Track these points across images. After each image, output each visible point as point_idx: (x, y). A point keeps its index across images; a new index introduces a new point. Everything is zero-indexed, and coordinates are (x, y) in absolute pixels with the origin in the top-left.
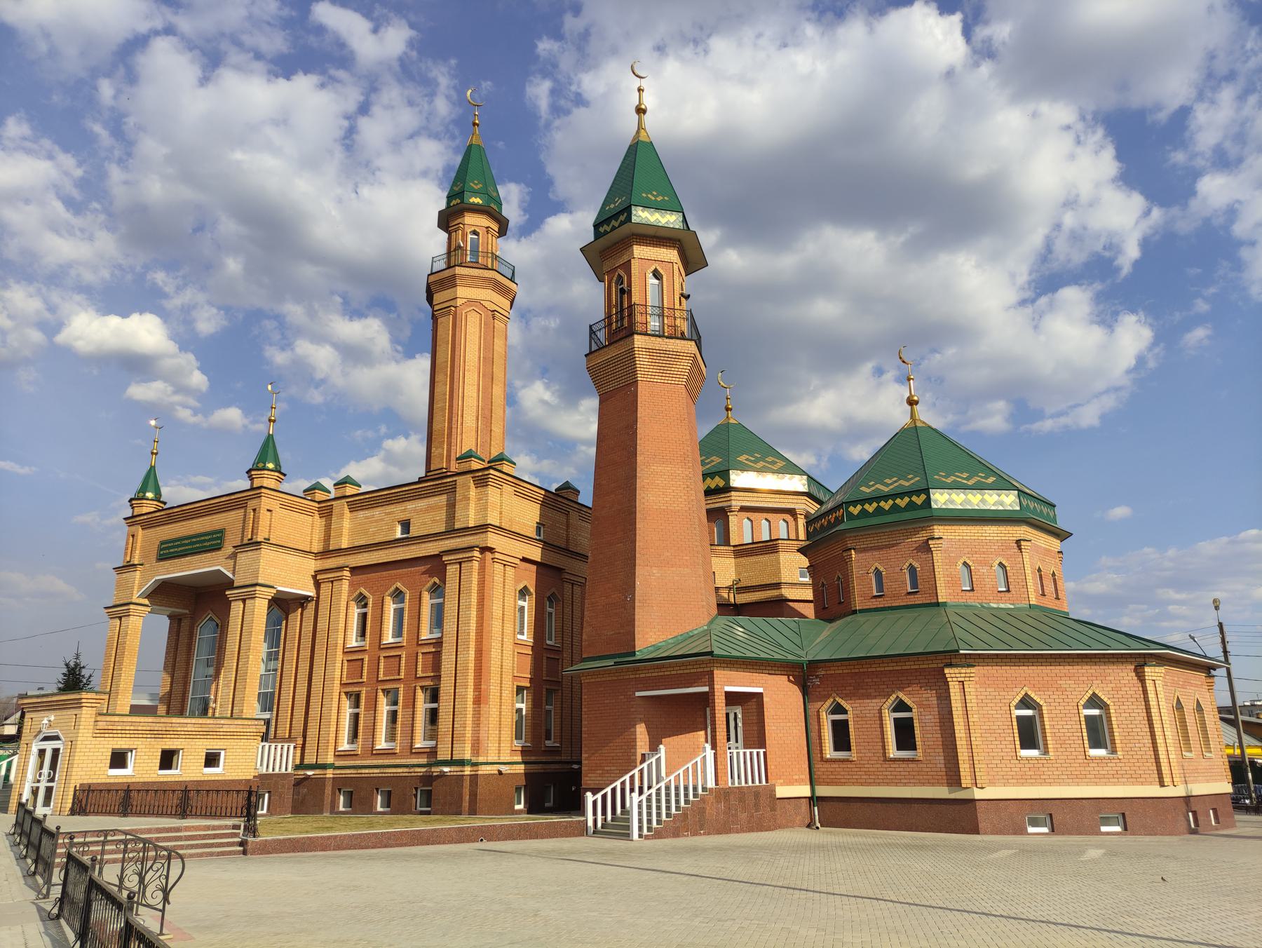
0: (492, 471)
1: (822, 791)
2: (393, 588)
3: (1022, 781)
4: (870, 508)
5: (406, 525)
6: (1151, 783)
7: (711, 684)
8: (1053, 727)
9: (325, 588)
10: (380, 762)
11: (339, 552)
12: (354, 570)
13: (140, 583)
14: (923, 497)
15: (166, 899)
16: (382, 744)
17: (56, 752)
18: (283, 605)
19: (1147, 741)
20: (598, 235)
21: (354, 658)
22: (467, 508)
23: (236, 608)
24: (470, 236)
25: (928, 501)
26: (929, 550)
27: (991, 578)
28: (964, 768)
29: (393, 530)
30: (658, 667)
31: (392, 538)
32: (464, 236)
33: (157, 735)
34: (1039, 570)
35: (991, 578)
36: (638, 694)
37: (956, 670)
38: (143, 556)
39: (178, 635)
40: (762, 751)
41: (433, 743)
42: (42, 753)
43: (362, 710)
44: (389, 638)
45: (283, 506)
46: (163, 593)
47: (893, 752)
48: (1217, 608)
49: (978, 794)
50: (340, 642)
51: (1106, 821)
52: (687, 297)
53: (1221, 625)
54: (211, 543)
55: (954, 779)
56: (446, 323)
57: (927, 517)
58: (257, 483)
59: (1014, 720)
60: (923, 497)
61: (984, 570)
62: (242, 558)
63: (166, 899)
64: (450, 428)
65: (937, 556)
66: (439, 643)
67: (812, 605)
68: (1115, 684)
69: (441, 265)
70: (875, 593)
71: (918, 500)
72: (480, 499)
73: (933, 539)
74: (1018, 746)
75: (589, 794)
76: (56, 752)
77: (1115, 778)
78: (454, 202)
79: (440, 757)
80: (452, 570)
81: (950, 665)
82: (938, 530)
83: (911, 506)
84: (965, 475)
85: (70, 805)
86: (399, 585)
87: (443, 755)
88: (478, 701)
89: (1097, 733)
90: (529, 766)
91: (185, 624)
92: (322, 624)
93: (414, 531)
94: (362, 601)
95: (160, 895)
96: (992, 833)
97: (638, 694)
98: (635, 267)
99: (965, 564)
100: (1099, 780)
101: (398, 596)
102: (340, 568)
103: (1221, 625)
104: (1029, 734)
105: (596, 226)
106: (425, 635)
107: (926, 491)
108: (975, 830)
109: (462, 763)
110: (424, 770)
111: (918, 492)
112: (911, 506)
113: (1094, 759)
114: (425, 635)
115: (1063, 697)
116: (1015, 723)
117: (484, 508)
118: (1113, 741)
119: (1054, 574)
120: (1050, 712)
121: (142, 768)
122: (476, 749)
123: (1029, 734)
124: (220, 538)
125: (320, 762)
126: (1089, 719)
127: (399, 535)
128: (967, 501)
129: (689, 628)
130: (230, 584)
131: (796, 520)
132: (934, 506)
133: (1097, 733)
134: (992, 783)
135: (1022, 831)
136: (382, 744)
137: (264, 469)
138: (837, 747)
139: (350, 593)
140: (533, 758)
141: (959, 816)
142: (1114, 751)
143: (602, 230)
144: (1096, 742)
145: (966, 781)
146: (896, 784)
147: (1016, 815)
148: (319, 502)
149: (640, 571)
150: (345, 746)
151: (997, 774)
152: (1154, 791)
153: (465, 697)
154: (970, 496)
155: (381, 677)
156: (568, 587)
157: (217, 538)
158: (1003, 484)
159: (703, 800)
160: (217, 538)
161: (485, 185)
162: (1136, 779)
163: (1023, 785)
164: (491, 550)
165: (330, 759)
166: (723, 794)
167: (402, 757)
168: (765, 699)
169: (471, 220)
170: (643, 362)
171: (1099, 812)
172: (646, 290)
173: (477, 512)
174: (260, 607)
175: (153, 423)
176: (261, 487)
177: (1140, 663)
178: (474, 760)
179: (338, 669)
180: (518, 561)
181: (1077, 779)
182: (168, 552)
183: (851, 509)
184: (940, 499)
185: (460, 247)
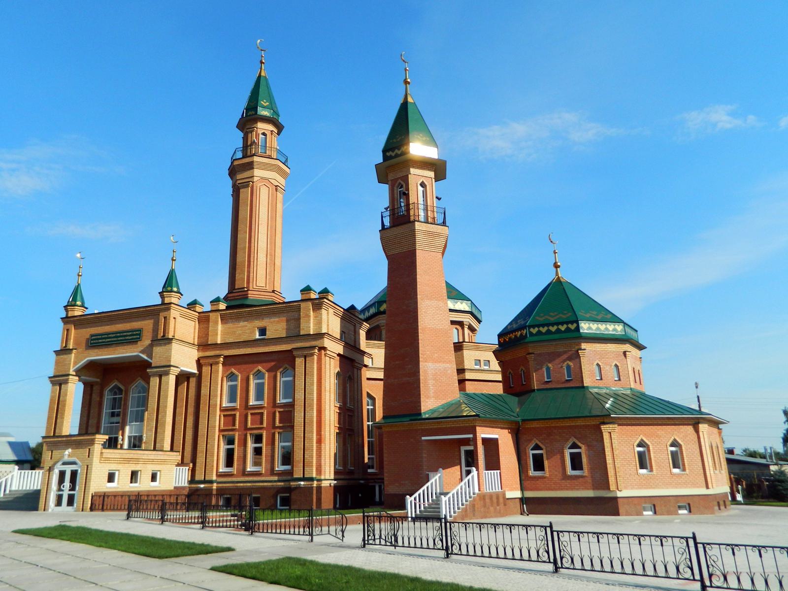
0: (325, 300)
1: (529, 494)
2: (255, 370)
3: (641, 487)
4: (544, 330)
5: (263, 331)
6: (702, 487)
7: (474, 432)
8: (655, 457)
9: (206, 370)
10: (250, 479)
11: (215, 346)
12: (226, 357)
13: (74, 362)
14: (575, 325)
15: (343, 536)
16: (250, 468)
17: (74, 474)
18: (183, 378)
19: (700, 464)
20: (386, 158)
21: (229, 414)
22: (309, 322)
23: (154, 381)
24: (261, 136)
25: (578, 329)
26: (578, 357)
27: (610, 373)
28: (612, 480)
29: (253, 332)
30: (438, 423)
31: (253, 338)
32: (257, 136)
33: (128, 460)
34: (634, 369)
35: (610, 373)
36: (423, 438)
37: (607, 426)
38: (75, 342)
39: (91, 395)
40: (498, 471)
41: (288, 467)
42: (62, 474)
43: (236, 446)
44: (252, 402)
45: (182, 316)
46: (91, 367)
47: (570, 471)
48: (697, 387)
49: (619, 494)
50: (218, 403)
51: (680, 507)
52: (439, 199)
53: (698, 397)
54: (133, 337)
55: (607, 487)
56: (245, 193)
57: (579, 338)
58: (167, 300)
59: (669, 453)
60: (575, 325)
61: (608, 368)
62: (157, 350)
63: (343, 536)
64: (249, 261)
65: (584, 361)
66: (292, 405)
67: (501, 384)
68: (684, 434)
69: (239, 155)
70: (546, 380)
71: (573, 327)
72: (316, 317)
73: (581, 349)
74: (638, 467)
75: (408, 497)
76: (74, 474)
77: (685, 485)
78: (250, 113)
79: (295, 476)
80: (299, 362)
81: (604, 423)
82: (583, 346)
83: (568, 330)
84: (595, 313)
85: (89, 505)
86: (260, 368)
87: (298, 474)
88: (319, 441)
89: (677, 461)
90: (341, 482)
91: (96, 389)
92: (204, 391)
93: (269, 335)
94: (231, 377)
95: (341, 533)
96: (626, 515)
97: (423, 438)
98: (411, 179)
99: (598, 365)
100: (677, 485)
101: (259, 375)
102: (219, 356)
103: (698, 397)
104: (643, 461)
105: (385, 151)
106: (280, 400)
107: (577, 322)
108: (618, 515)
109: (312, 479)
110: (282, 484)
111: (572, 322)
112: (568, 330)
113: (675, 475)
114: (280, 400)
115: (660, 440)
116: (637, 455)
117: (319, 323)
118: (684, 465)
119: (639, 371)
120: (654, 449)
121: (122, 484)
122: (319, 471)
123: (643, 461)
124: (139, 334)
125: (207, 479)
126: (672, 452)
127: (257, 337)
128: (598, 329)
129: (449, 400)
130: (148, 365)
131: (463, 329)
132: (581, 331)
133: (677, 461)
134: (626, 488)
135: (642, 514)
136: (250, 468)
137: (172, 291)
138: (574, 468)
139: (224, 372)
140: (342, 477)
141: (608, 506)
142: (684, 470)
143: (388, 154)
144: (642, 465)
145: (613, 487)
146: (572, 489)
147: (639, 504)
148: (199, 313)
149: (422, 365)
150: (222, 469)
151: (627, 483)
152: (703, 491)
153: (311, 439)
154: (600, 325)
155: (249, 425)
156: (355, 370)
157: (137, 335)
158: (616, 320)
159: (474, 499)
160: (137, 335)
161: (271, 103)
162: (695, 485)
163: (640, 488)
164: (325, 349)
165: (214, 478)
166: (482, 497)
167: (237, 476)
168: (499, 442)
169: (262, 126)
170: (420, 238)
171: (678, 502)
172: (416, 194)
173: (315, 325)
174: (172, 380)
175: (78, 255)
176: (171, 303)
177: (695, 424)
178: (318, 477)
179: (217, 420)
180: (336, 355)
181: (667, 485)
182: (94, 343)
183: (532, 330)
184: (586, 327)
185: (254, 142)
